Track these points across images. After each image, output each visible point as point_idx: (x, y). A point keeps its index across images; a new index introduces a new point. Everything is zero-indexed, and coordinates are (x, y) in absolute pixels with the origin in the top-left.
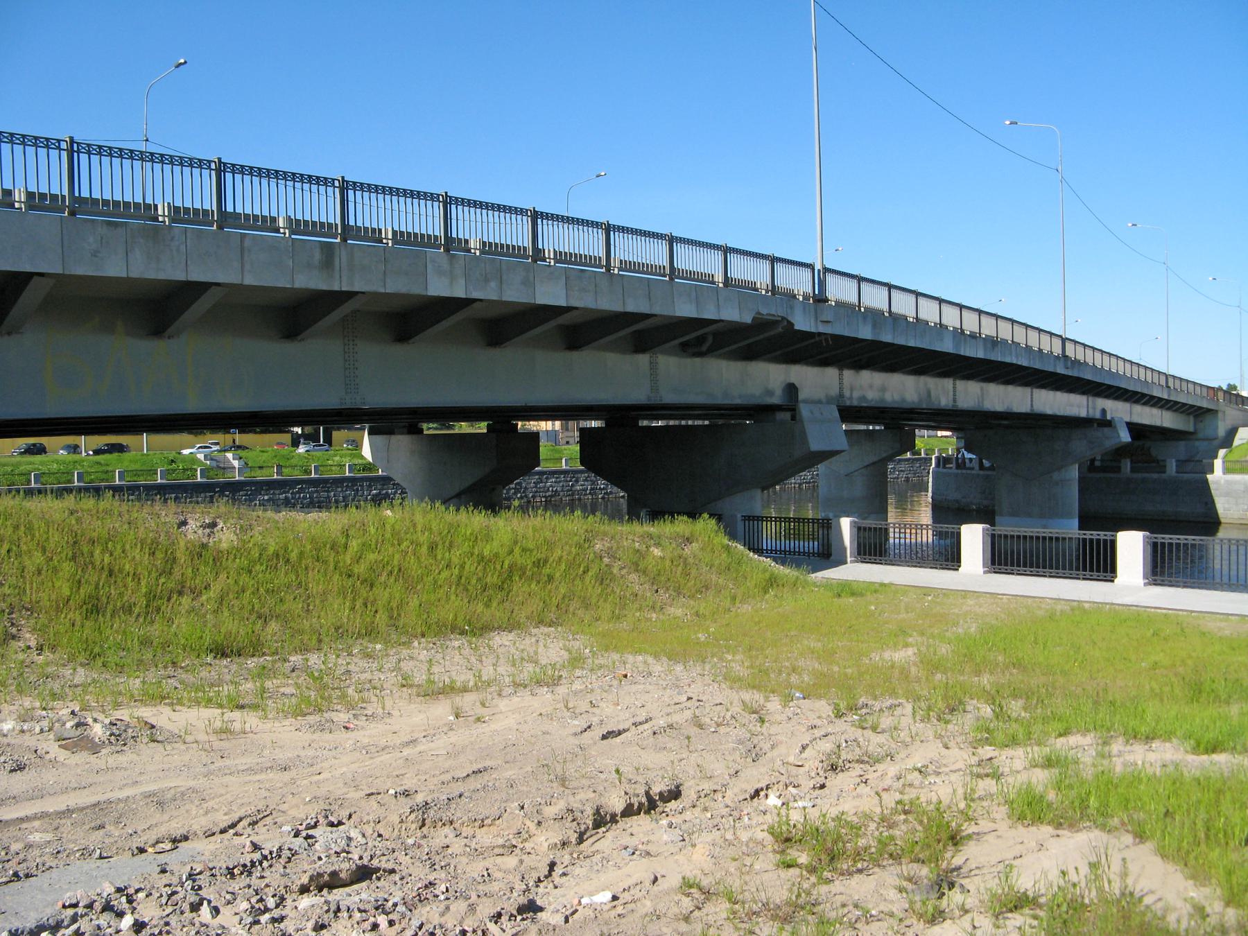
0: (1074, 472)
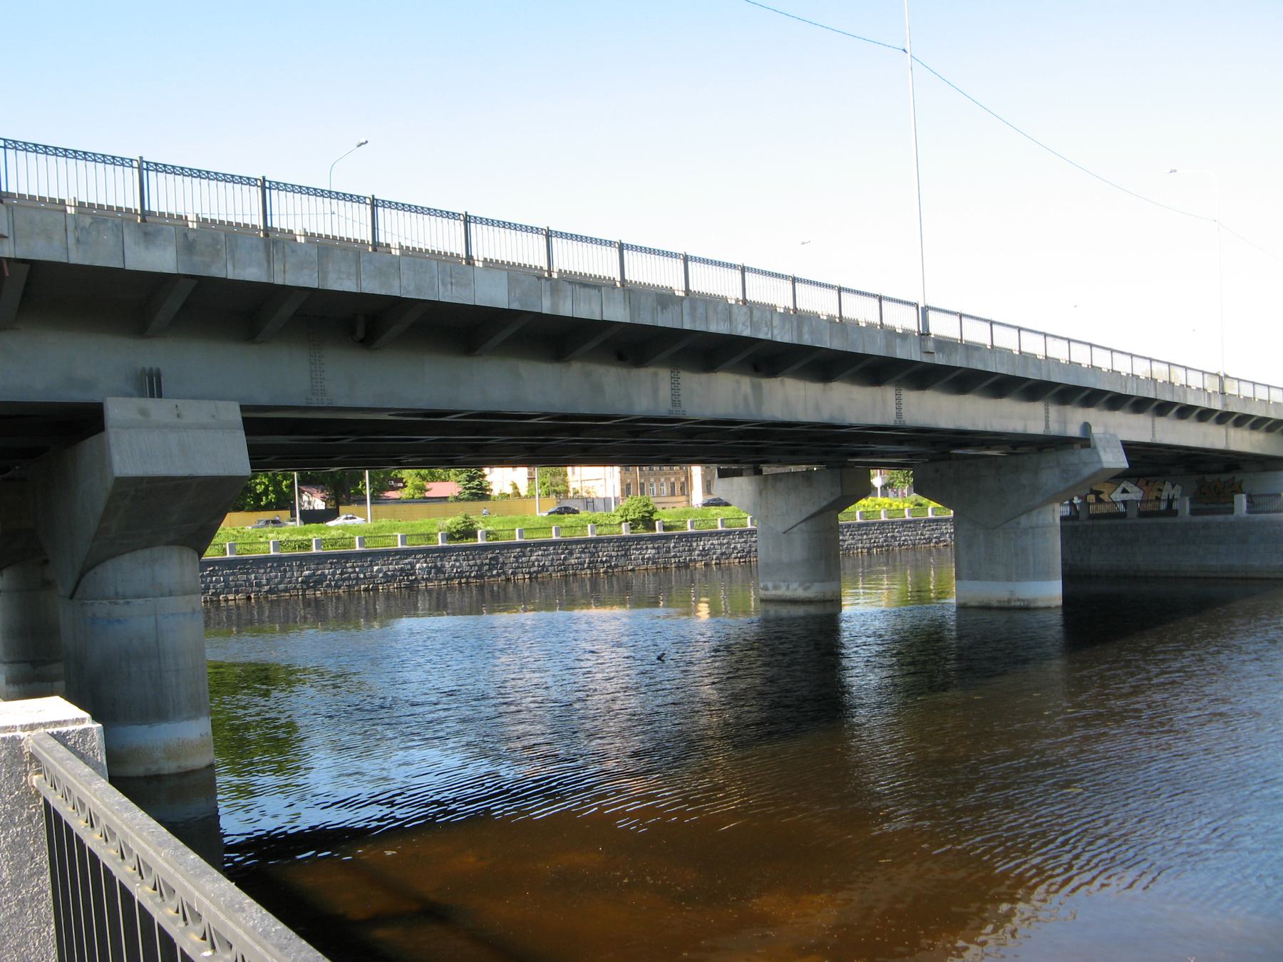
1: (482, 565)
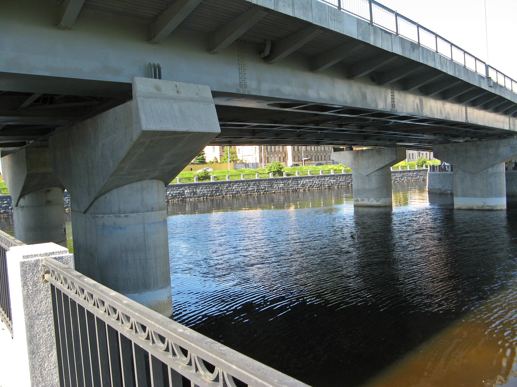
0: (502, 168)
1: (213, 191)
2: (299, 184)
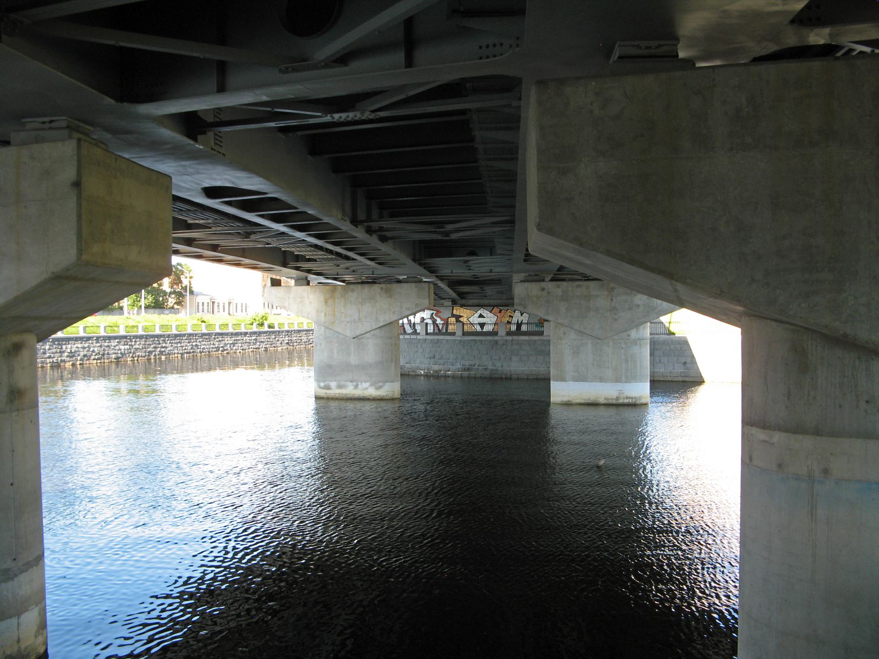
2: (64, 352)
